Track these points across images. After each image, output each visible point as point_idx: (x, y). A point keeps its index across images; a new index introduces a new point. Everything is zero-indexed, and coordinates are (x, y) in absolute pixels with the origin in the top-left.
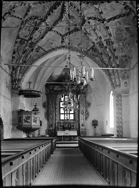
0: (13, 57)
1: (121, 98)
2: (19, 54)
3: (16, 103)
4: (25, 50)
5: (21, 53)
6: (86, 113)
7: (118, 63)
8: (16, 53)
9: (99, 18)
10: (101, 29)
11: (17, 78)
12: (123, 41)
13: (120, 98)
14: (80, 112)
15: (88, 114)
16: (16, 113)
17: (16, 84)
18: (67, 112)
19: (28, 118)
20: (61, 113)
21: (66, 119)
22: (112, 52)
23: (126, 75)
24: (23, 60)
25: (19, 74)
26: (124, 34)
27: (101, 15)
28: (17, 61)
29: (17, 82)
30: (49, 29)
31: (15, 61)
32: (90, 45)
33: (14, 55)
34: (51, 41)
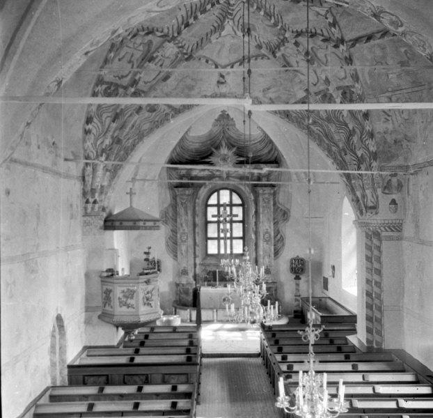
0: (87, 132)
1: (381, 243)
2: (101, 123)
3: (94, 253)
4: (118, 111)
5: (108, 121)
6: (275, 237)
7: (373, 149)
8: (95, 120)
9: (326, 33)
10: (329, 60)
11: (98, 186)
12: (387, 94)
13: (375, 241)
14: (262, 237)
15: (282, 239)
16: (96, 280)
17: (95, 202)
18: (225, 235)
19: (131, 294)
20: (210, 235)
21: (222, 252)
22: (357, 119)
23: (394, 180)
24: (112, 137)
25: (104, 175)
26: (395, 76)
27: (333, 29)
28: (96, 140)
29: (99, 195)
30: (186, 56)
31: (92, 141)
32: (295, 95)
33: (90, 126)
34: (189, 81)
